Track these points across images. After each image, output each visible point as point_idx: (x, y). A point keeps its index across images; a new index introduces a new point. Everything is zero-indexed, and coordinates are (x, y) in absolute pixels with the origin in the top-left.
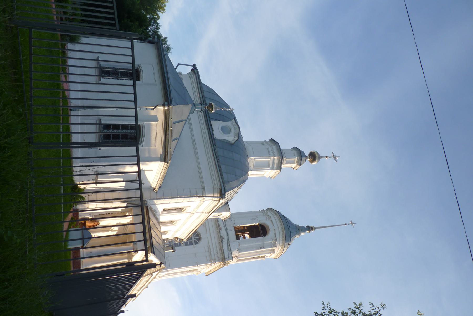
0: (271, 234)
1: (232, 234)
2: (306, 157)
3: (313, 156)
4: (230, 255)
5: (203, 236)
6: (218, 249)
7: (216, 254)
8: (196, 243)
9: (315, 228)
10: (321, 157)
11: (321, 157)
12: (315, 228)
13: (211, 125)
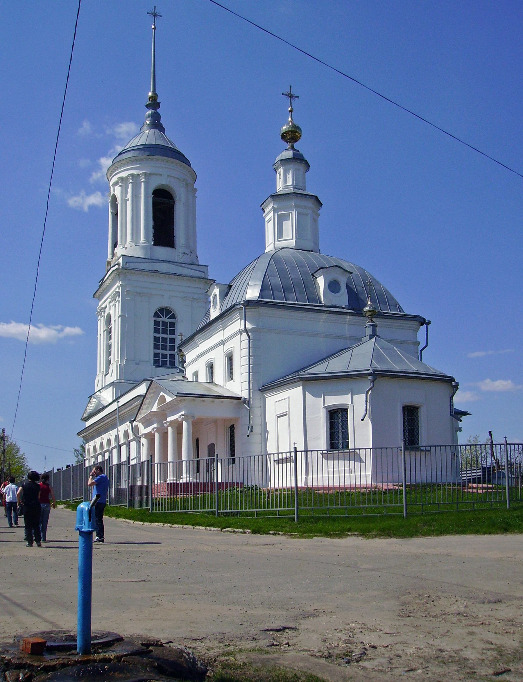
1: (162, 252)
4: (201, 268)
5: (165, 303)
8: (173, 317)
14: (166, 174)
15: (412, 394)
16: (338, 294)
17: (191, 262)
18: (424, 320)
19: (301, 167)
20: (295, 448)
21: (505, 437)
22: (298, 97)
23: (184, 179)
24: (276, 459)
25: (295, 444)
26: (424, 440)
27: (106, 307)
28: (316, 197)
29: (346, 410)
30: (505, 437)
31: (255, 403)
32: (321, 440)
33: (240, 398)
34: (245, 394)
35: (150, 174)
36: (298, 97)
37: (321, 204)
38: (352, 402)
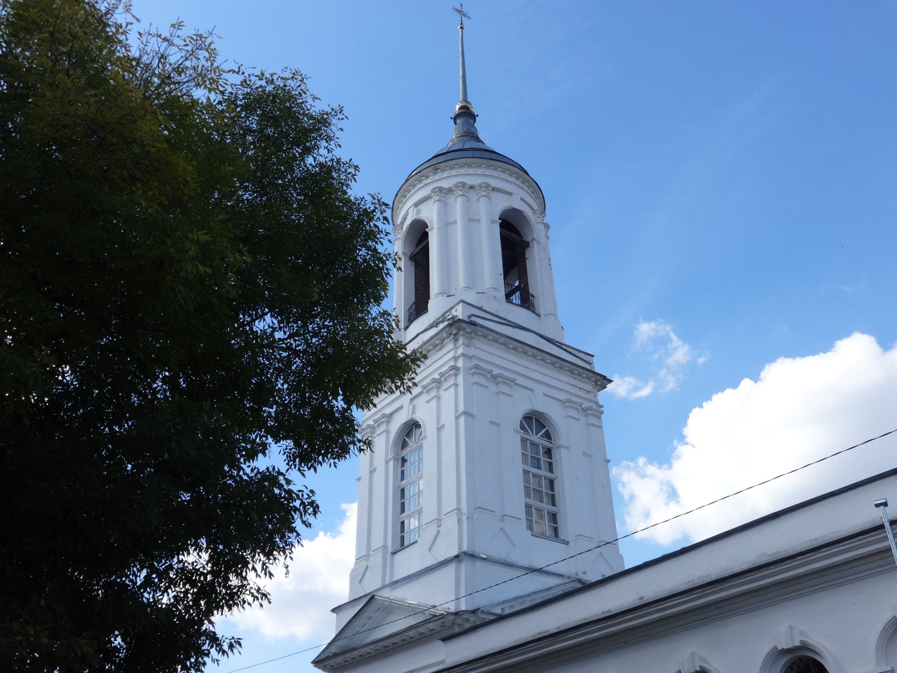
6: (572, 381)
7: (581, 393)
27: (401, 407)
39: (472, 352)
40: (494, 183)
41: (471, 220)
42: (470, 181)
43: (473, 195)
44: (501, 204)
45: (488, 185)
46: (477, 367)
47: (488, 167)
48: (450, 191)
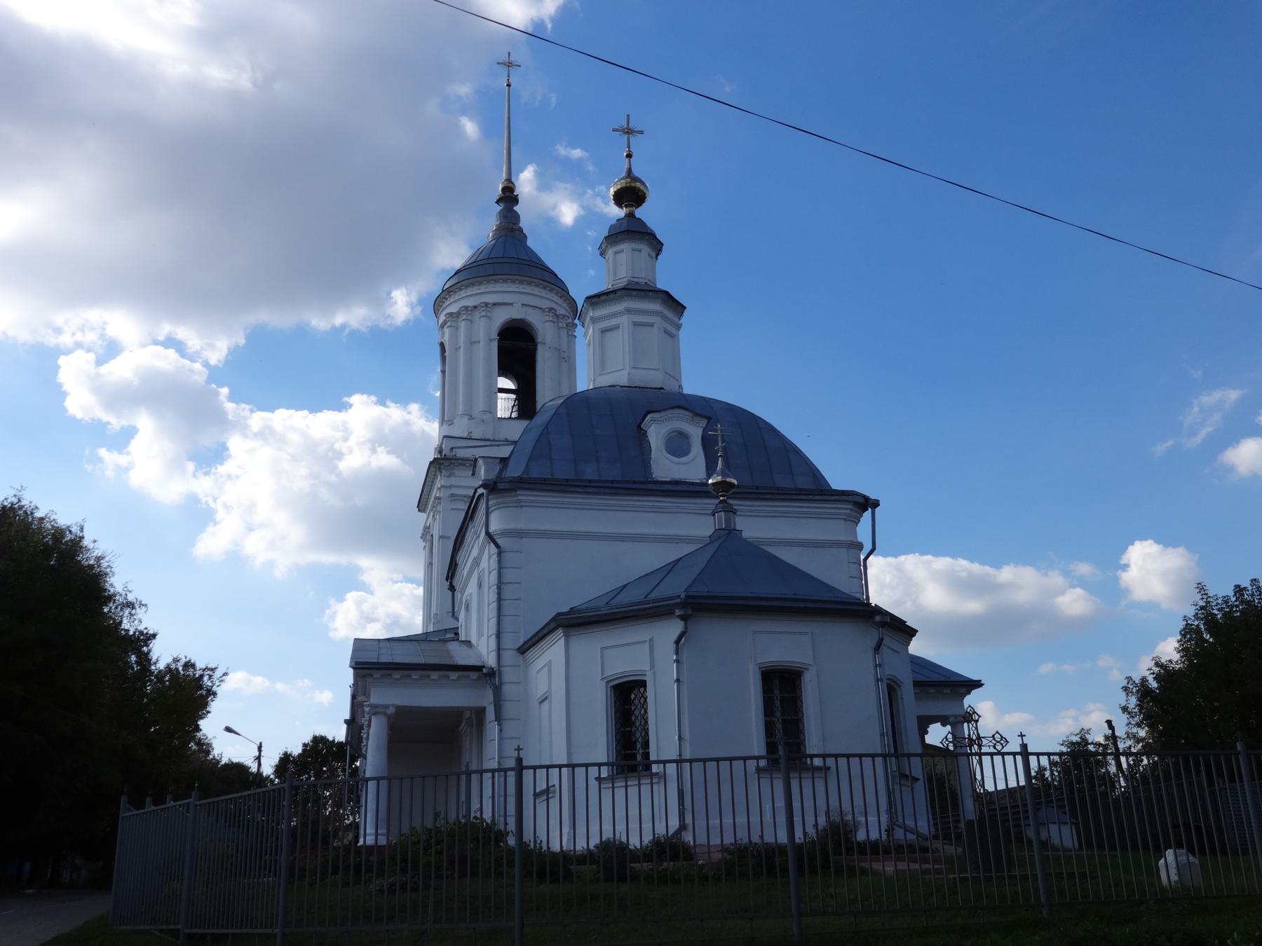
0: (537, 320)
2: (630, 215)
3: (630, 195)
9: (509, 180)
10: (630, 171)
11: (630, 171)
12: (509, 180)
13: (677, 483)
14: (516, 301)
15: (784, 643)
16: (676, 459)
17: (465, 435)
18: (866, 498)
19: (645, 249)
20: (519, 760)
21: (1022, 736)
22: (642, 132)
23: (551, 309)
24: (542, 786)
25: (519, 749)
26: (813, 743)
28: (667, 293)
29: (643, 684)
30: (1022, 736)
31: (508, 675)
32: (597, 744)
33: (478, 669)
34: (491, 661)
35: (494, 304)
36: (642, 132)
37: (678, 308)
38: (652, 666)
39: (453, 481)
40: (491, 299)
41: (472, 343)
42: (470, 303)
43: (477, 315)
44: (501, 317)
45: (486, 304)
46: (452, 495)
47: (489, 282)
48: (458, 314)
